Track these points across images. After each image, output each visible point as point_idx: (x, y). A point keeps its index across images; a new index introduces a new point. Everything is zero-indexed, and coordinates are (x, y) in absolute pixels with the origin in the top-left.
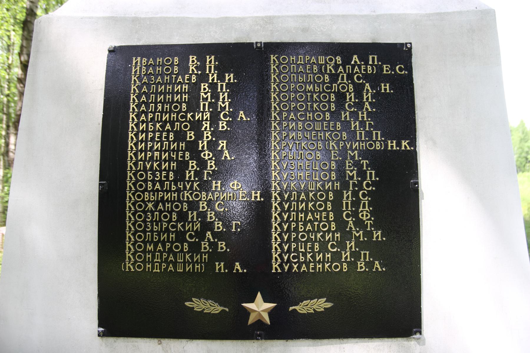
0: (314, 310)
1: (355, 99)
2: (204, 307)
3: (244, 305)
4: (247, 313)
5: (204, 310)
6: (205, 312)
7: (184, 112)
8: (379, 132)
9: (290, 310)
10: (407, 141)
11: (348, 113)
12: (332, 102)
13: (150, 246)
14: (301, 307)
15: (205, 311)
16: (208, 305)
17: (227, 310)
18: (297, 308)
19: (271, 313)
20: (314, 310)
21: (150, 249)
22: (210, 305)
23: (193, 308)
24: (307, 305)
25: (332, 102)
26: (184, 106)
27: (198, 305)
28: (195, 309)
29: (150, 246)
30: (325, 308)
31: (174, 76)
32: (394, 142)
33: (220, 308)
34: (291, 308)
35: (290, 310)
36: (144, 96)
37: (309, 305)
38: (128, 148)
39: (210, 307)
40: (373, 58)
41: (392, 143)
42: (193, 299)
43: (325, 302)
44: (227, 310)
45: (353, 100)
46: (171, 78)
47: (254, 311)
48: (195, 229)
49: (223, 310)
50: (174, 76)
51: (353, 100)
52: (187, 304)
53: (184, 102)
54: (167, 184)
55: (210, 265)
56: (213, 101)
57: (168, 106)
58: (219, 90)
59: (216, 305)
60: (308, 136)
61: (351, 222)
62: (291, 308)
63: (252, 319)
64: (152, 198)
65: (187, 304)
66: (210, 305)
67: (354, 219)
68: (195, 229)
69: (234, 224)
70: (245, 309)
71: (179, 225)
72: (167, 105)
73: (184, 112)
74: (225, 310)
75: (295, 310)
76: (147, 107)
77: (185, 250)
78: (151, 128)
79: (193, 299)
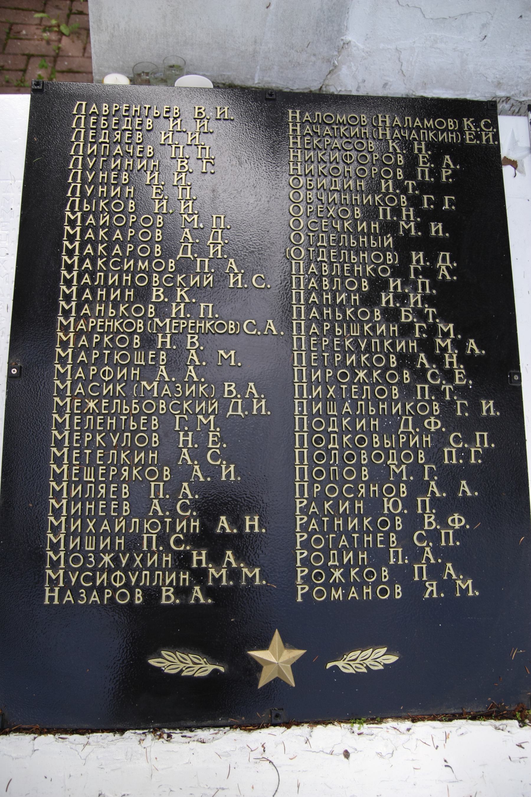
0: (367, 667)
1: (425, 261)
2: (182, 666)
4: (257, 667)
5: (182, 671)
7: (171, 273)
9: (327, 667)
10: (471, 119)
14: (346, 662)
15: (184, 674)
16: (189, 661)
18: (340, 664)
19: (297, 667)
20: (367, 667)
21: (143, 268)
27: (172, 662)
30: (385, 665)
31: (124, 418)
33: (211, 668)
34: (329, 665)
35: (327, 667)
39: (191, 665)
40: (482, 437)
42: (163, 653)
44: (222, 669)
45: (422, 263)
46: (118, 420)
47: (269, 663)
49: (215, 671)
50: (124, 418)
51: (422, 263)
52: (152, 662)
59: (202, 662)
61: (428, 549)
62: (329, 665)
63: (264, 680)
70: (253, 659)
73: (171, 273)
79: (163, 653)
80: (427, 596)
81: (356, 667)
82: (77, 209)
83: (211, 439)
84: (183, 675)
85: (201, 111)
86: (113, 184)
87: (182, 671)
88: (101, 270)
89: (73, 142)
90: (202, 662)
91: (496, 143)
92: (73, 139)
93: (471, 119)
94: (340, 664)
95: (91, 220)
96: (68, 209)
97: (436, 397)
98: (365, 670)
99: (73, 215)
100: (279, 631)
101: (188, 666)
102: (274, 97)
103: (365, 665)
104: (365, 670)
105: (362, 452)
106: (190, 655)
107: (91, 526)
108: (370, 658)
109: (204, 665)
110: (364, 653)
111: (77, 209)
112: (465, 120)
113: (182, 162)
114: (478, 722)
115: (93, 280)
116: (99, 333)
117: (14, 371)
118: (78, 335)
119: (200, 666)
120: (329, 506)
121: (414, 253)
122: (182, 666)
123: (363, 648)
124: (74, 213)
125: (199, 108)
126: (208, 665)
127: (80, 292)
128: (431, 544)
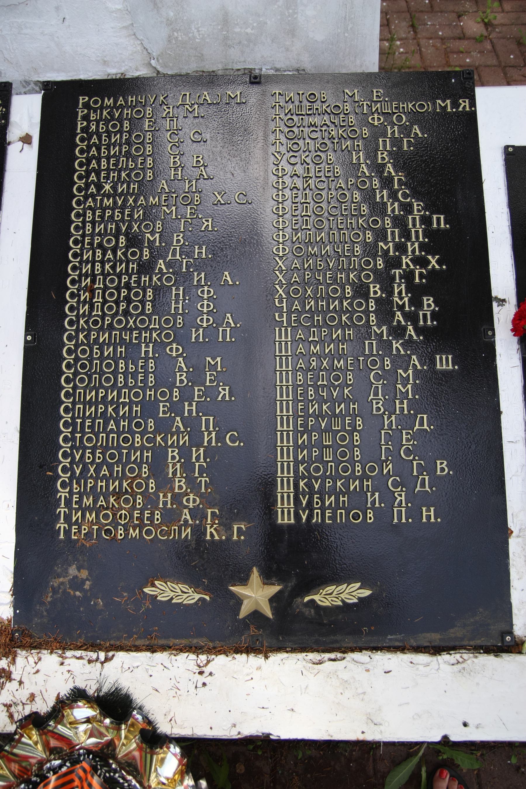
0: (343, 601)
5: (172, 599)
6: (174, 601)
13: (109, 100)
14: (322, 596)
15: (174, 601)
16: (179, 591)
18: (316, 598)
20: (343, 601)
26: (145, 469)
28: (158, 598)
29: (109, 100)
30: (359, 599)
33: (197, 596)
36: (93, 174)
37: (335, 593)
38: (77, 118)
39: (180, 593)
42: (156, 582)
43: (358, 589)
44: (207, 598)
53: (146, 463)
55: (184, 478)
58: (203, 429)
59: (190, 591)
60: (340, 250)
63: (245, 611)
69: (221, 331)
70: (233, 595)
74: (204, 599)
76: (99, 149)
78: (97, 353)
79: (156, 582)
80: (220, 399)
81: (332, 600)
84: (174, 601)
85: (199, 159)
86: (112, 169)
87: (172, 599)
90: (190, 591)
91: (473, 109)
94: (316, 598)
97: (411, 350)
98: (340, 603)
100: (268, 619)
101: (177, 594)
102: (258, 80)
103: (340, 599)
104: (340, 603)
106: (179, 585)
107: (92, 471)
108: (346, 592)
109: (192, 594)
113: (174, 158)
114: (445, 658)
117: (29, 338)
119: (187, 595)
120: (304, 484)
125: (198, 157)
126: (196, 594)
128: (404, 489)
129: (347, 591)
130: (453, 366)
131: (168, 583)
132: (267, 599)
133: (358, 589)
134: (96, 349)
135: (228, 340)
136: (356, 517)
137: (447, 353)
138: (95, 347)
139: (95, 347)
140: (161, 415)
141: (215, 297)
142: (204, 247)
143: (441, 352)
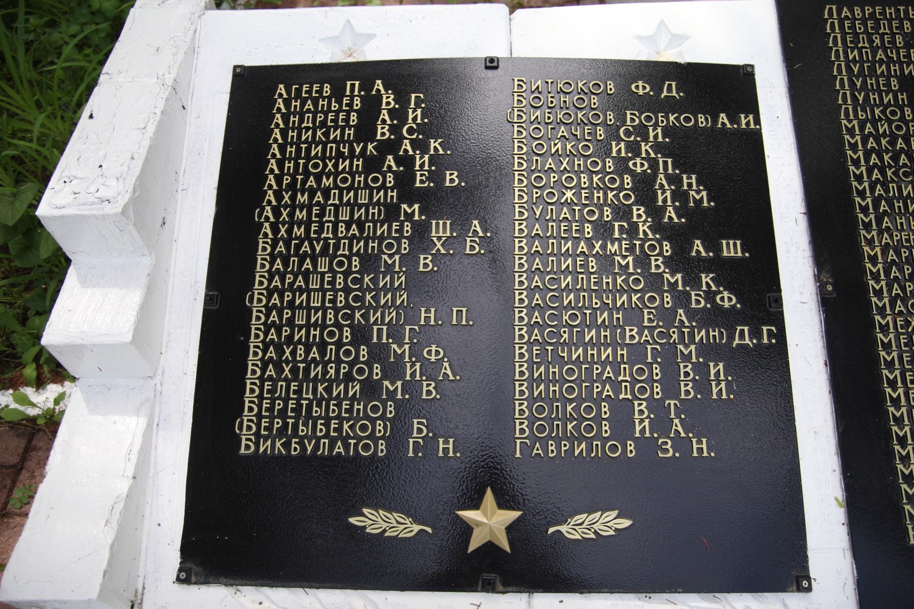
0: (596, 533)
2: (385, 525)
3: (460, 513)
4: (467, 530)
5: (385, 531)
6: (386, 535)
8: (670, 161)
10: (711, 275)
11: (622, 145)
12: (604, 419)
14: (570, 526)
16: (393, 521)
17: (429, 530)
18: (563, 529)
20: (596, 533)
22: (397, 521)
23: (365, 527)
24: (582, 524)
25: (604, 419)
28: (367, 530)
30: (616, 530)
32: (694, 176)
33: (416, 528)
34: (551, 530)
37: (586, 523)
39: (395, 524)
41: (689, 178)
42: (365, 511)
43: (615, 519)
44: (429, 530)
47: (479, 524)
48: (387, 320)
52: (352, 520)
54: (324, 443)
56: (423, 217)
57: (362, 179)
59: (407, 521)
62: (551, 530)
64: (303, 431)
65: (352, 520)
66: (397, 521)
67: (652, 416)
68: (387, 320)
71: (366, 279)
72: (360, 177)
75: (559, 531)
77: (388, 185)
78: (295, 449)
79: (365, 511)
82: (852, 117)
83: (646, 317)
84: (386, 535)
87: (385, 531)
88: (893, 181)
89: (831, 48)
91: (758, 127)
92: (831, 45)
93: (711, 275)
94: (563, 529)
95: (869, 128)
96: (842, 117)
99: (850, 123)
105: (339, 275)
110: (591, 517)
111: (852, 117)
112: (703, 276)
115: (887, 191)
116: (906, 247)
118: (885, 249)
119: (403, 526)
121: (742, 116)
122: (385, 525)
123: (590, 512)
124: (850, 121)
127: (877, 202)
129: (601, 521)
130: (743, 252)
131: (380, 511)
132: (503, 528)
133: (615, 519)
134: (295, 443)
135: (464, 323)
136: (614, 448)
137: (735, 238)
138: (294, 440)
139: (294, 440)
140: (418, 184)
141: (431, 435)
142: (433, 310)
143: (727, 238)
